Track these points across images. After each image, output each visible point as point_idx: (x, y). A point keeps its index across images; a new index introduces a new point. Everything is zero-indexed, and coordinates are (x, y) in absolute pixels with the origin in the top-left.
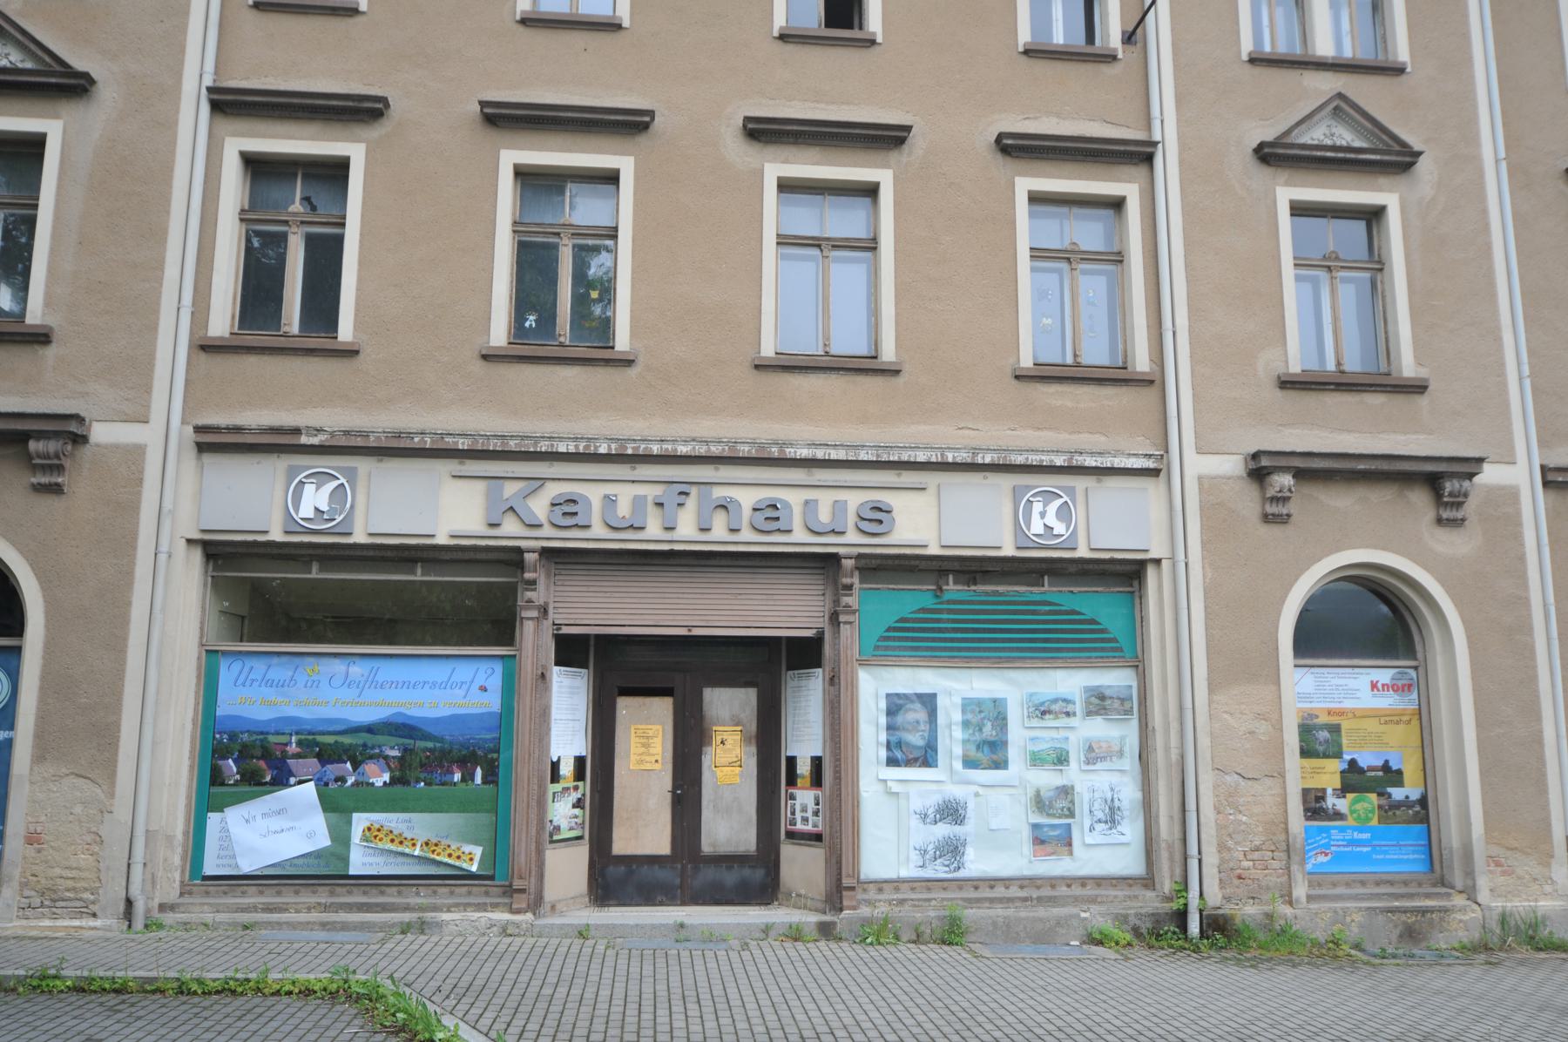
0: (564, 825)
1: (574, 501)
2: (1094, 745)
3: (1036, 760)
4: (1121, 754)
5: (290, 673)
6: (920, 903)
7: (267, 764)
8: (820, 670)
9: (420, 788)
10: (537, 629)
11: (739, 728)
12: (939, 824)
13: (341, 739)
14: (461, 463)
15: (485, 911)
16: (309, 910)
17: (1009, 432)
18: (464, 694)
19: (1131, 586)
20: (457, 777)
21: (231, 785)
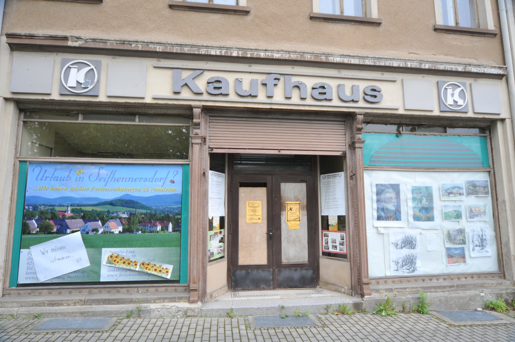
0: (215, 251)
1: (219, 81)
2: (473, 209)
3: (447, 217)
4: (484, 212)
5: (67, 173)
6: (401, 290)
7: (54, 222)
8: (342, 174)
9: (139, 234)
10: (201, 149)
11: (298, 202)
12: (404, 249)
13: (95, 208)
14: (158, 61)
15: (175, 301)
16: (75, 304)
17: (433, 56)
18: (162, 184)
19: (485, 133)
20: (159, 228)
21: (34, 234)
